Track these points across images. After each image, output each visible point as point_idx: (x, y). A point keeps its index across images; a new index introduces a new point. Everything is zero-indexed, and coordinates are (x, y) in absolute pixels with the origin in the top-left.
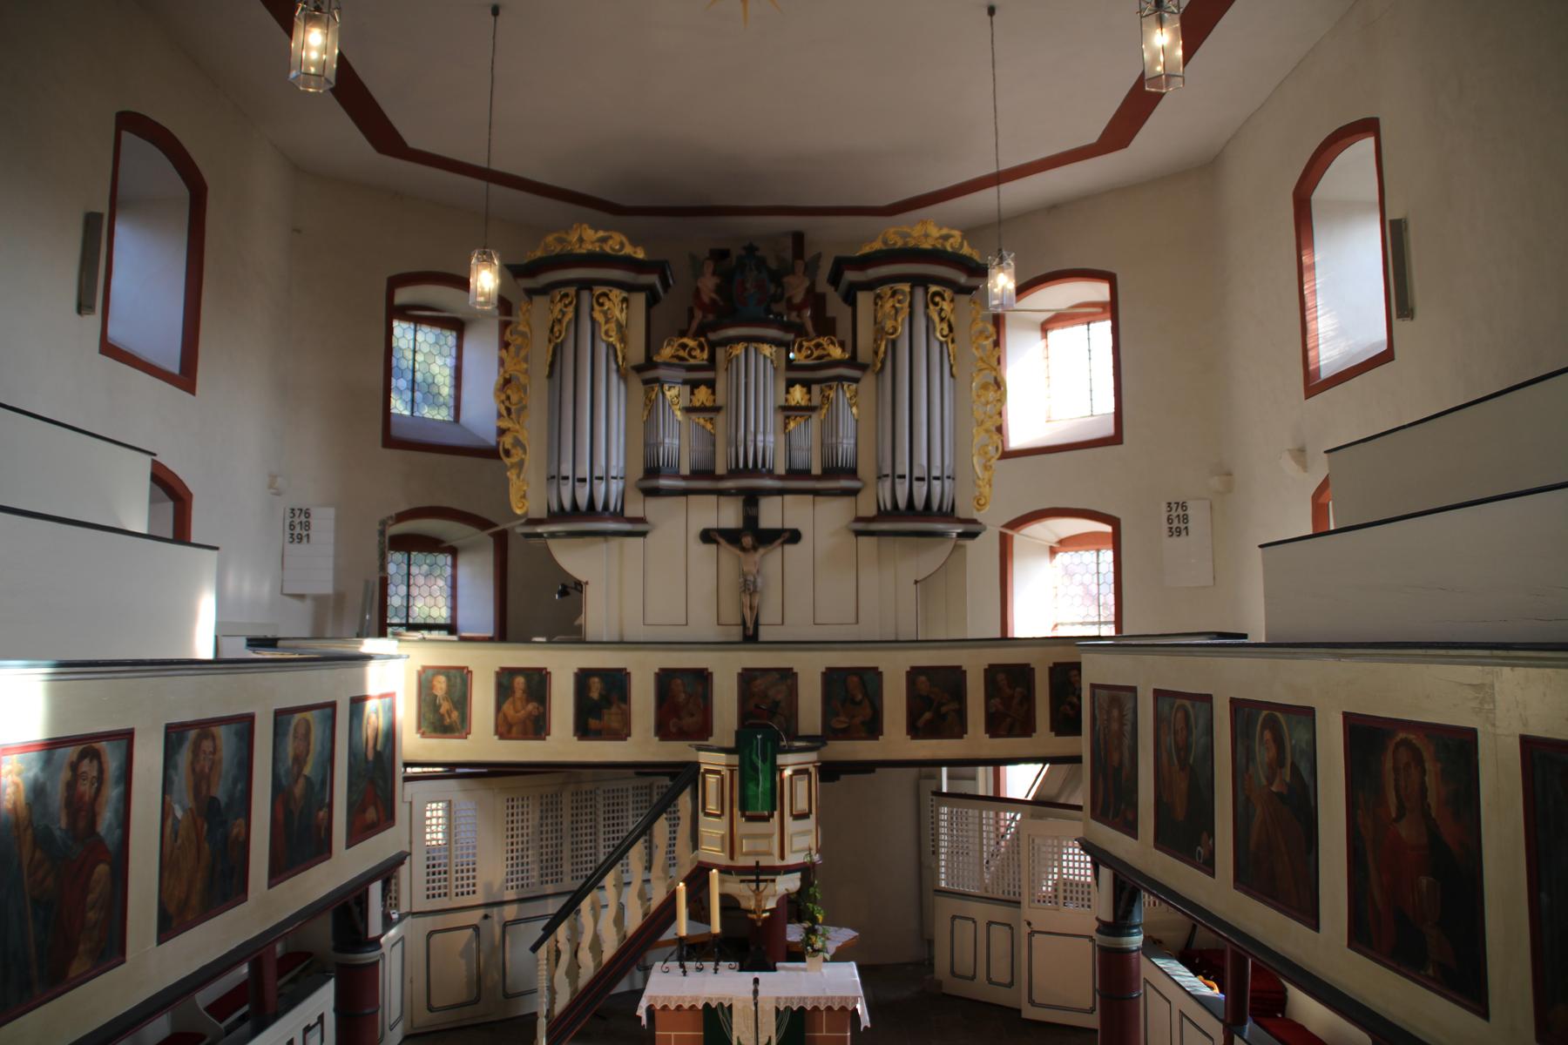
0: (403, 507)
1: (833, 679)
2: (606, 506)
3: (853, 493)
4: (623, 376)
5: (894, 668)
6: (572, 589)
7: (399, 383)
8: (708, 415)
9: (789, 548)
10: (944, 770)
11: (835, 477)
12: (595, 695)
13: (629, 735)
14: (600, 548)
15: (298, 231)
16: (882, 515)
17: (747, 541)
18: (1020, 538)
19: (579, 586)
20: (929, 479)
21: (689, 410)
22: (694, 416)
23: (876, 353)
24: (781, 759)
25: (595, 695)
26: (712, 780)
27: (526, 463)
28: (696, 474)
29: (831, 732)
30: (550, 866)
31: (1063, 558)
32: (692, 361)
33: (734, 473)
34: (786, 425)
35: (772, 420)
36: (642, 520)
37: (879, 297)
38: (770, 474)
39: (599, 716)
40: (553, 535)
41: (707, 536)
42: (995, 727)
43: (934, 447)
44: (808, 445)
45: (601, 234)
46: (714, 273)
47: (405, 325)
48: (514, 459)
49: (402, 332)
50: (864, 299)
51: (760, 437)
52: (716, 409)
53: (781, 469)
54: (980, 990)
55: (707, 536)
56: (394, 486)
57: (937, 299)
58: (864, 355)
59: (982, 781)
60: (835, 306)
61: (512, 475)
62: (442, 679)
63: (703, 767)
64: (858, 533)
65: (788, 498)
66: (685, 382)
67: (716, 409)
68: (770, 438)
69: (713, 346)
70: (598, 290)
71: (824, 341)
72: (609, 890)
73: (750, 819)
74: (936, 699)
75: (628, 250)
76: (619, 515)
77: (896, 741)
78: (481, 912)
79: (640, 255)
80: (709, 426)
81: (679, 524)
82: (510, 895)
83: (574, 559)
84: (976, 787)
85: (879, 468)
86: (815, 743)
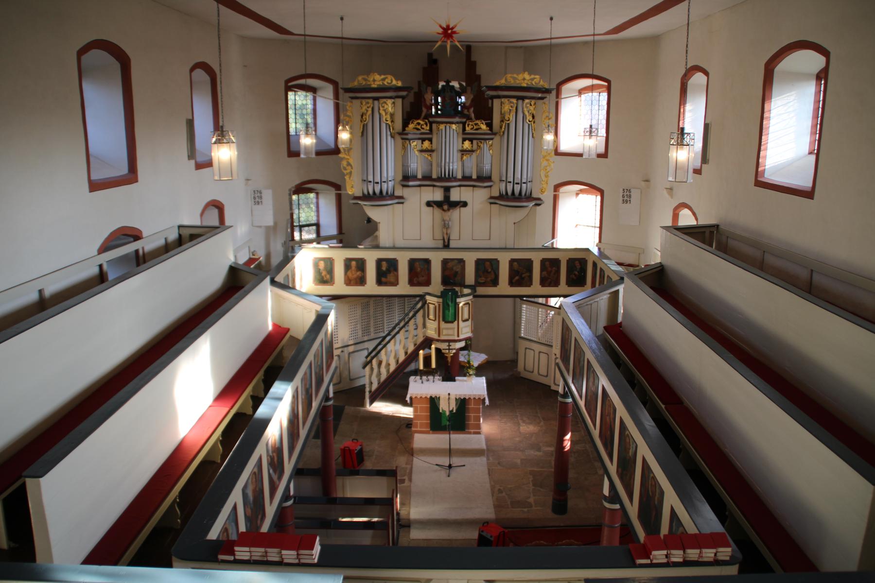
4: (392, 137)
9: (462, 209)
11: (484, 179)
12: (384, 268)
15: (245, 66)
17: (446, 207)
22: (423, 154)
23: (501, 127)
24: (458, 300)
25: (384, 268)
29: (478, 284)
30: (366, 330)
32: (423, 131)
33: (440, 179)
34: (462, 158)
35: (456, 155)
38: (455, 179)
39: (386, 277)
41: (429, 204)
42: (544, 282)
43: (525, 171)
44: (471, 166)
48: (348, 171)
52: (432, 151)
53: (459, 176)
54: (535, 377)
55: (429, 204)
64: (491, 203)
67: (432, 151)
69: (431, 123)
71: (478, 122)
72: (390, 346)
74: (521, 272)
75: (394, 82)
77: (504, 287)
78: (340, 350)
79: (400, 84)
81: (418, 198)
82: (351, 342)
83: (374, 213)
85: (501, 177)
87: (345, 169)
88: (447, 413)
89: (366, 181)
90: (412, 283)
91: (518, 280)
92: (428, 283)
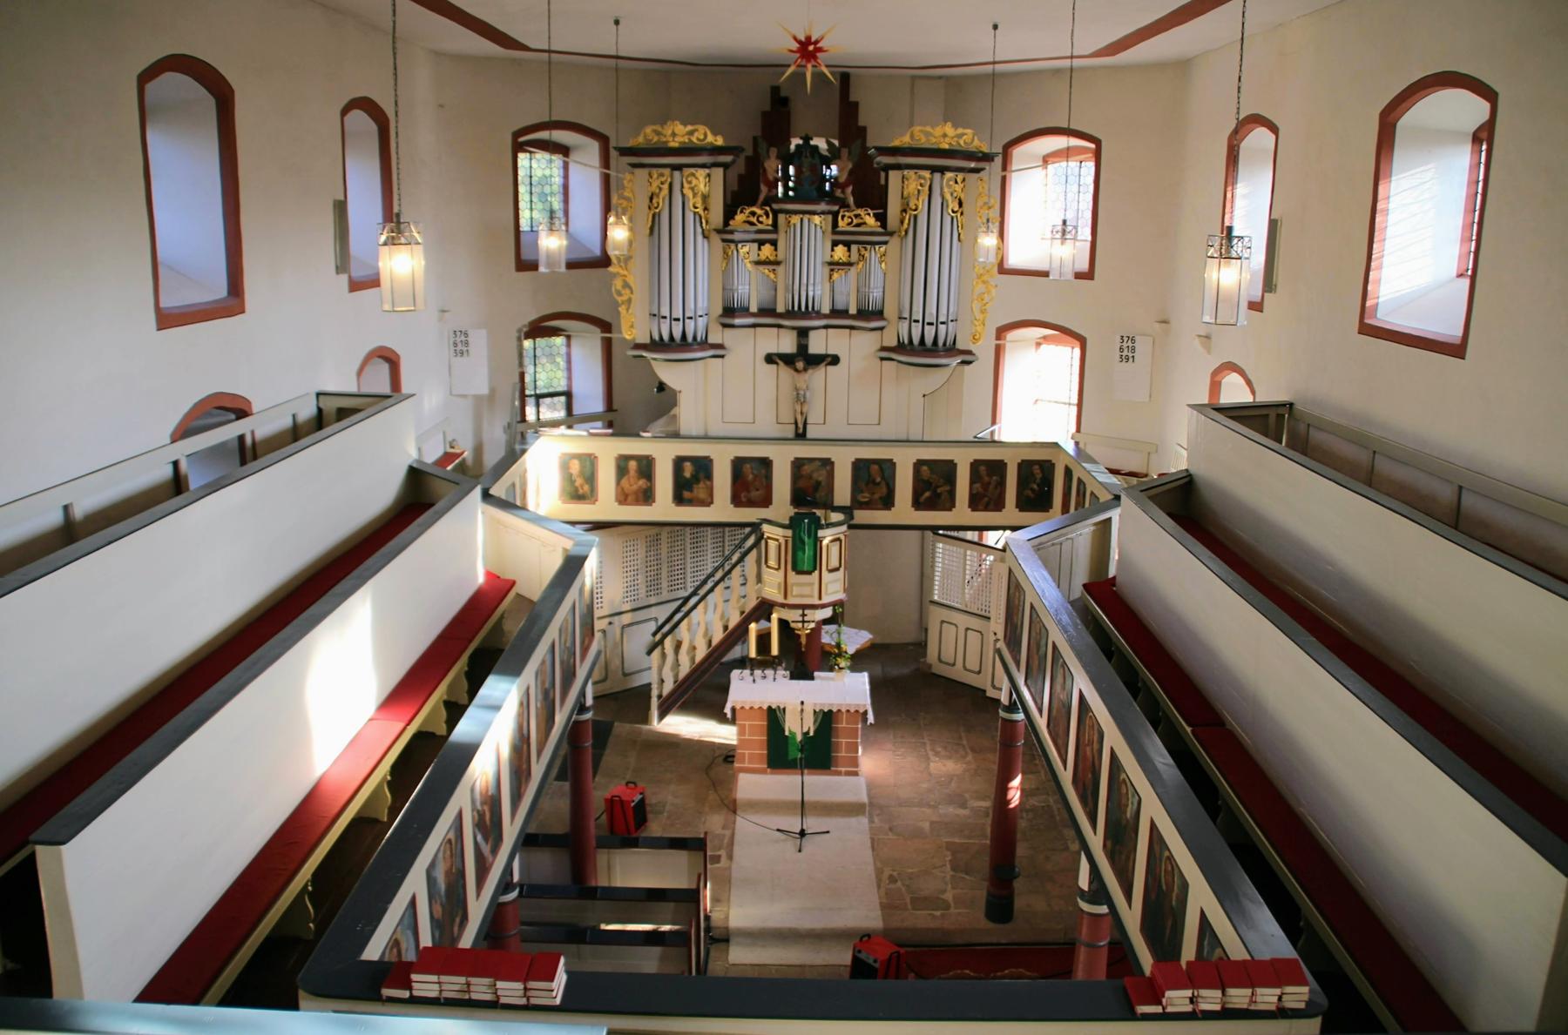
1: (861, 468)
2: (695, 338)
5: (905, 462)
9: (830, 368)
12: (687, 474)
15: (441, 106)
17: (800, 365)
20: (937, 324)
22: (761, 268)
24: (821, 533)
25: (687, 474)
29: (857, 504)
30: (653, 585)
32: (760, 227)
33: (790, 314)
35: (821, 272)
36: (721, 346)
41: (770, 359)
42: (976, 503)
48: (625, 298)
52: (778, 263)
53: (826, 310)
54: (958, 674)
55: (770, 359)
61: (622, 309)
64: (882, 359)
69: (776, 213)
71: (861, 212)
74: (934, 485)
75: (710, 138)
77: (903, 510)
78: (607, 620)
79: (720, 141)
81: (750, 347)
82: (627, 607)
83: (669, 372)
85: (900, 312)
87: (619, 294)
88: (799, 738)
90: (737, 501)
91: (929, 498)
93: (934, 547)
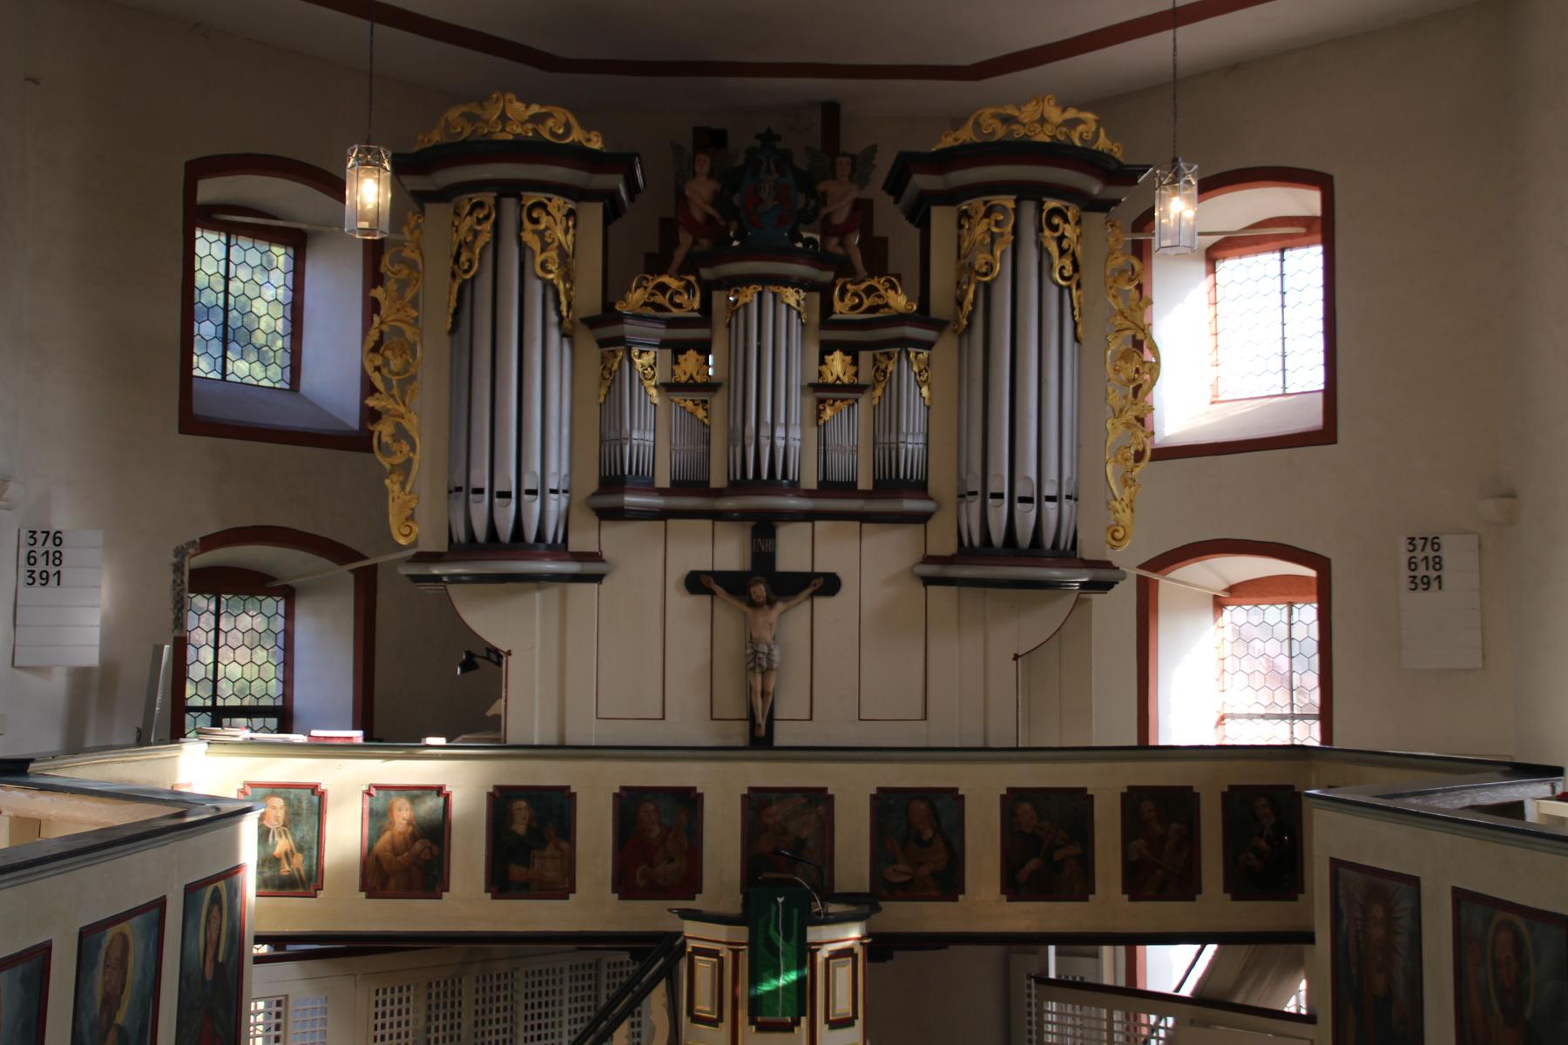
0: (213, 528)
2: (540, 536)
3: (922, 518)
5: (982, 790)
6: (485, 662)
7: (206, 329)
8: (699, 396)
9: (820, 602)
10: (1052, 949)
11: (891, 495)
13: (572, 890)
14: (539, 601)
15: (35, 81)
16: (965, 553)
17: (760, 591)
18: (1169, 585)
19: (496, 656)
20: (1040, 499)
21: (668, 388)
22: (677, 397)
24: (813, 934)
25: (520, 828)
26: (704, 966)
27: (415, 467)
28: (679, 487)
31: (1235, 615)
32: (676, 313)
33: (738, 486)
35: (798, 405)
36: (596, 557)
37: (965, 215)
38: (794, 488)
40: (455, 579)
41: (696, 583)
42: (1137, 883)
43: (1046, 448)
44: (851, 441)
45: (535, 109)
46: (710, 176)
47: (212, 236)
49: (209, 247)
50: (942, 218)
51: (780, 432)
53: (810, 481)
55: (696, 583)
56: (199, 493)
57: (1056, 220)
58: (940, 305)
59: (1108, 965)
60: (890, 219)
61: (392, 484)
62: (278, 802)
63: (691, 944)
64: (928, 581)
65: (820, 525)
66: (663, 345)
67: (711, 387)
68: (795, 433)
69: (708, 289)
70: (531, 198)
71: (879, 283)
73: (763, 1028)
74: (1047, 845)
75: (577, 135)
76: (559, 549)
77: (985, 904)
79: (596, 144)
80: (701, 413)
81: (651, 563)
83: (489, 619)
84: (1098, 971)
86: (861, 905)
87: (388, 453)
89: (462, 491)
90: (625, 885)
92: (690, 884)
93: (1041, 1012)
